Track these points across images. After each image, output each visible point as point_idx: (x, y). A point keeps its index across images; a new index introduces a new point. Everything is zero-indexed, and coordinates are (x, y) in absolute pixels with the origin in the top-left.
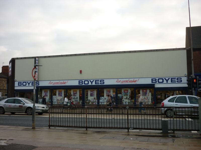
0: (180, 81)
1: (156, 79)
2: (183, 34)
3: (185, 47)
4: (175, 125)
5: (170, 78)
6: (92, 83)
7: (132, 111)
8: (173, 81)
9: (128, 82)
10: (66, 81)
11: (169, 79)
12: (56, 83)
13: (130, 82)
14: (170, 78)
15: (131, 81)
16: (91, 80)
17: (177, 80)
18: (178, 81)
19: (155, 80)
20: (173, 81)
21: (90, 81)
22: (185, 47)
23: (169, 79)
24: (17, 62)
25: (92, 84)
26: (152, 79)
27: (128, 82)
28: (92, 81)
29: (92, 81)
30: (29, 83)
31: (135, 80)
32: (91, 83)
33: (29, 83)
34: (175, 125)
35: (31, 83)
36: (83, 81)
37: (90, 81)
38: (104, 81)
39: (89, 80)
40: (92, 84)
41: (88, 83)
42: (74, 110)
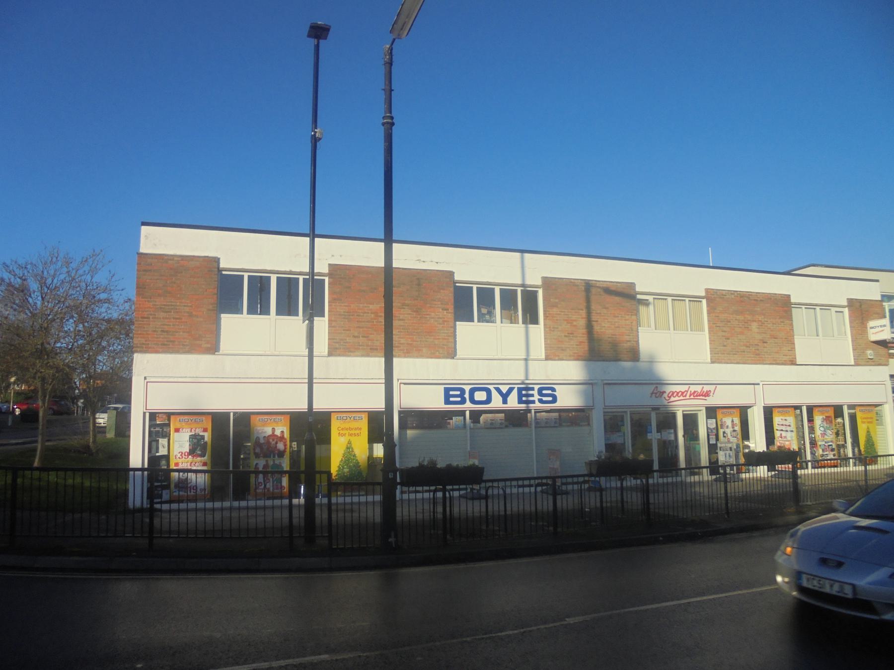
0: (550, 399)
1: (463, 391)
2: (309, 39)
4: (817, 480)
5: (514, 388)
6: (505, 397)
7: (628, 485)
8: (451, 399)
9: (685, 396)
10: (712, 388)
11: (510, 390)
12: (678, 393)
13: (692, 397)
14: (514, 388)
15: (695, 392)
16: (501, 387)
17: (540, 391)
18: (545, 399)
19: (458, 393)
20: (451, 399)
21: (498, 390)
23: (510, 390)
24: (841, 314)
25: (505, 402)
26: (447, 391)
27: (688, 397)
28: (504, 389)
29: (504, 389)
30: (504, 392)
31: (705, 390)
32: (501, 399)
33: (504, 392)
34: (817, 480)
35: (515, 392)
36: (467, 388)
37: (498, 390)
38: (553, 390)
39: (491, 387)
40: (505, 402)
41: (489, 400)
42: (607, 486)
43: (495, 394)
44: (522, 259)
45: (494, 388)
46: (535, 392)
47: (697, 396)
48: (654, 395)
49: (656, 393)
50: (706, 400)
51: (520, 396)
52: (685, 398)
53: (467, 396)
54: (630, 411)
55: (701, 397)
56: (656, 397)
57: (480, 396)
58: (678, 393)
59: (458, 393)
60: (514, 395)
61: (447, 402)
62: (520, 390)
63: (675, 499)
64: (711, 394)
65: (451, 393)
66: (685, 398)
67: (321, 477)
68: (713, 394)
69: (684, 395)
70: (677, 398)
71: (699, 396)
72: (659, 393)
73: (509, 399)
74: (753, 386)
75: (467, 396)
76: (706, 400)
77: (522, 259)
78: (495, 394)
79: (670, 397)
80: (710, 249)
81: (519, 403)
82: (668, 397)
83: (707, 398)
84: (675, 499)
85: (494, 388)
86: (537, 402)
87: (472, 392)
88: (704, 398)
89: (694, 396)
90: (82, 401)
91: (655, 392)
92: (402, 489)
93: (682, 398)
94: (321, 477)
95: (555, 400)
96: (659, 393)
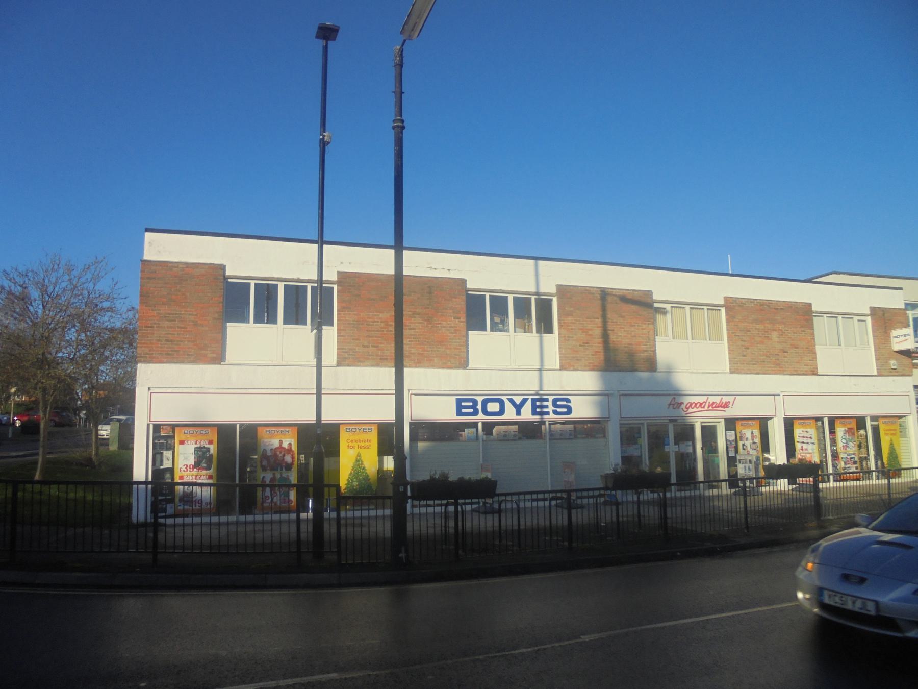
0: (565, 410)
1: (475, 402)
3: (404, 251)
4: (839, 494)
5: (528, 399)
6: (518, 408)
7: (645, 499)
8: (464, 411)
9: (704, 407)
10: (731, 399)
11: (524, 402)
12: (696, 404)
13: (711, 408)
14: (528, 399)
15: (713, 403)
16: (514, 398)
17: (554, 403)
18: (559, 410)
19: (471, 404)
20: (464, 411)
21: (512, 401)
22: (404, 251)
23: (524, 402)
25: (518, 413)
26: (459, 402)
27: (706, 408)
28: (518, 400)
29: (518, 400)
30: (518, 403)
31: (724, 401)
32: (514, 410)
33: (518, 403)
34: (839, 494)
35: (529, 403)
36: (480, 399)
37: (512, 401)
38: (568, 401)
39: (504, 398)
40: (518, 413)
41: (502, 412)
42: (624, 500)
43: (508, 405)
44: (536, 266)
45: (507, 399)
46: (550, 404)
47: (715, 407)
48: (671, 406)
49: (674, 404)
50: (725, 411)
51: (534, 407)
52: (703, 409)
53: (479, 407)
54: (647, 423)
55: (720, 409)
56: (674, 408)
57: (493, 407)
58: (696, 404)
59: (471, 404)
60: (528, 406)
61: (459, 413)
62: (534, 401)
63: (693, 513)
64: (730, 405)
65: (463, 404)
66: (703, 409)
67: (329, 490)
68: (733, 405)
69: (703, 406)
70: (695, 409)
71: (718, 407)
72: (677, 404)
73: (523, 410)
74: (773, 397)
75: (479, 407)
76: (725, 411)
77: (536, 266)
78: (508, 405)
79: (688, 408)
80: (729, 256)
81: (533, 415)
82: (686, 408)
83: (725, 409)
84: (693, 513)
85: (507, 399)
86: (551, 413)
87: (485, 403)
88: (722, 409)
89: (712, 408)
90: (84, 412)
91: (673, 403)
92: (413, 503)
93: (700, 409)
94: (329, 490)
95: (569, 411)
96: (677, 404)
